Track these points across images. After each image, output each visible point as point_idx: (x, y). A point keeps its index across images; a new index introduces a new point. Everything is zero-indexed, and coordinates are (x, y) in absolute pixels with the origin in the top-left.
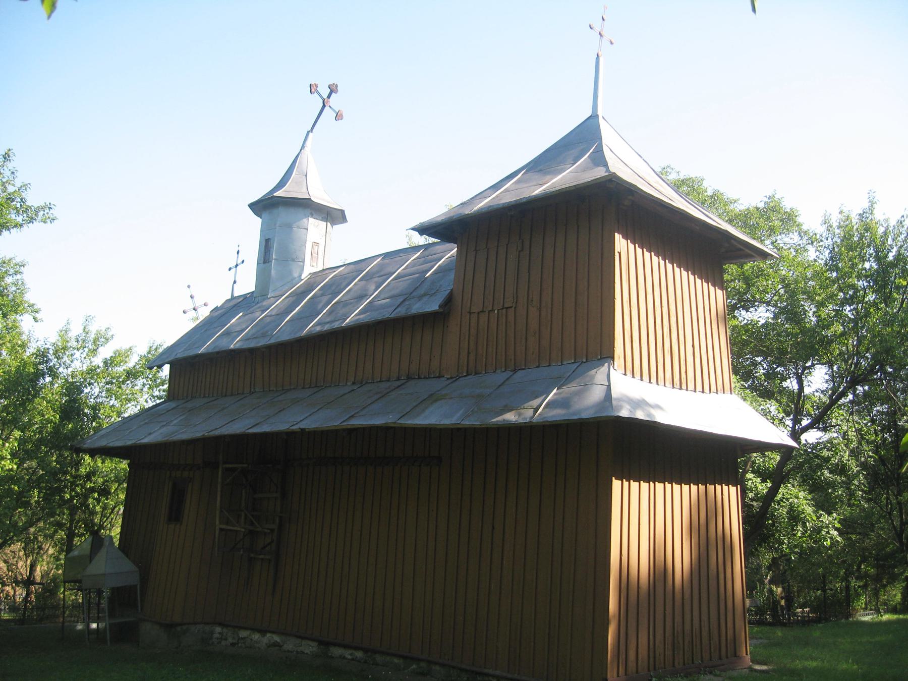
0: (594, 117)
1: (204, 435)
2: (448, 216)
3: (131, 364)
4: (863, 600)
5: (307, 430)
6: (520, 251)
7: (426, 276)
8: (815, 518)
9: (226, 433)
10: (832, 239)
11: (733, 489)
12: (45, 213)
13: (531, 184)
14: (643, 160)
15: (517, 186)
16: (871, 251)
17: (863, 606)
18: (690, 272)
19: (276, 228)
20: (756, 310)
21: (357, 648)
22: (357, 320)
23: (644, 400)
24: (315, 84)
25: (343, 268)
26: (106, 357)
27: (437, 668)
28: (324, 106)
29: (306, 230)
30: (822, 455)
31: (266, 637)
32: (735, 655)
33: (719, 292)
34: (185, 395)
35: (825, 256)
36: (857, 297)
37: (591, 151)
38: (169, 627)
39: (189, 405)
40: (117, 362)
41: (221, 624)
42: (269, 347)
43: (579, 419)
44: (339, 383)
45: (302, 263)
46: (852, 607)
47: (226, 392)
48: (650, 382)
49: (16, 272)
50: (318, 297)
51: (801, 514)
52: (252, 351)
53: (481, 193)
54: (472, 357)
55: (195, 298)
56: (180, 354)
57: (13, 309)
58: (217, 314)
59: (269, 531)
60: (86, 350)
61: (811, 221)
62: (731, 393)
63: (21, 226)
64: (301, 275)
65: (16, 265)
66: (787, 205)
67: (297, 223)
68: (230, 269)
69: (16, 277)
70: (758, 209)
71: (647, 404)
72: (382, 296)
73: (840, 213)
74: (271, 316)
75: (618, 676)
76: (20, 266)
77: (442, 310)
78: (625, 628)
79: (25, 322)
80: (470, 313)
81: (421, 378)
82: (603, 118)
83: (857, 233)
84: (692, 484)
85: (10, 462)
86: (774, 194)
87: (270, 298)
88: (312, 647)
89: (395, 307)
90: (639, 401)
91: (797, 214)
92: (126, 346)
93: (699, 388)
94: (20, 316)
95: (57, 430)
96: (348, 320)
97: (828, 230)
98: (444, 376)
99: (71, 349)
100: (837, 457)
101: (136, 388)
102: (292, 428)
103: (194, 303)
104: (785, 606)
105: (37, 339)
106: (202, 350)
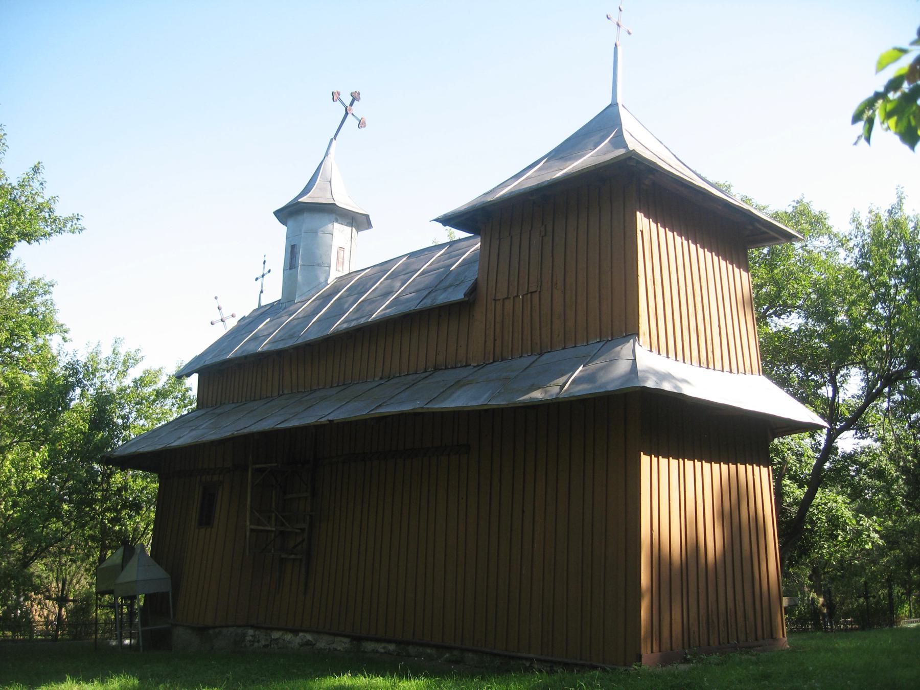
0: (614, 105)
1: (233, 434)
2: (471, 205)
3: (159, 385)
4: (907, 607)
5: (335, 422)
6: (543, 237)
7: (452, 269)
8: (854, 522)
9: (255, 430)
10: (861, 237)
11: (764, 470)
12: (74, 224)
13: (552, 170)
14: (664, 146)
15: (538, 174)
16: (902, 248)
17: (907, 614)
18: (714, 253)
19: (301, 234)
20: (788, 316)
21: (389, 641)
22: (384, 314)
23: (670, 374)
24: (338, 92)
25: (369, 270)
26: (136, 377)
27: (470, 655)
28: (347, 114)
30: (860, 460)
31: (298, 637)
32: (772, 638)
33: (744, 274)
34: (214, 402)
35: (854, 254)
36: (889, 294)
37: (611, 136)
38: (201, 630)
39: (218, 411)
40: (147, 382)
42: (297, 349)
43: (606, 392)
44: (366, 380)
45: (328, 268)
46: (896, 614)
47: (255, 396)
48: (676, 360)
49: (45, 291)
50: (344, 298)
51: (840, 518)
53: (504, 183)
54: (498, 343)
55: (222, 310)
56: (209, 361)
57: (43, 329)
58: (244, 323)
59: (299, 531)
61: (840, 224)
62: (759, 375)
63: (50, 234)
64: (327, 280)
65: (45, 285)
66: (815, 209)
67: (322, 229)
68: (257, 279)
69: (45, 298)
70: (786, 213)
71: (673, 378)
72: (408, 291)
73: (869, 212)
74: (298, 319)
75: (652, 652)
76: (49, 286)
77: (467, 299)
78: (657, 603)
79: (54, 341)
81: (449, 369)
83: (887, 230)
84: (722, 463)
85: (41, 472)
86: (802, 198)
87: (297, 303)
88: (345, 643)
90: (665, 374)
91: (826, 217)
92: (156, 367)
93: (727, 368)
94: (50, 336)
95: (88, 437)
96: (374, 316)
97: (857, 228)
98: (471, 365)
99: (101, 370)
100: (876, 462)
101: (166, 407)
104: (826, 614)
105: (66, 353)
106: (230, 356)
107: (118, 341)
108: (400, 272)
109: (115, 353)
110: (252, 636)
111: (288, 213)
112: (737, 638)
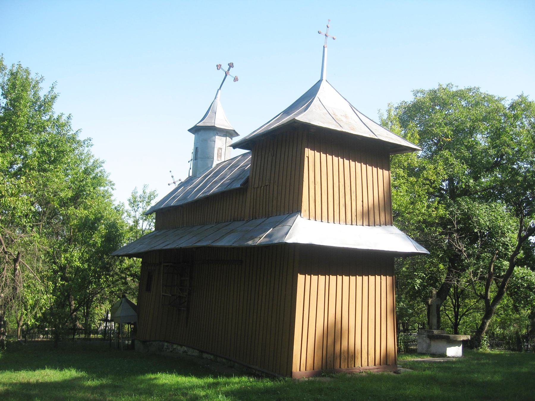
21: (211, 354)
24: (219, 65)
28: (226, 75)
29: (214, 142)
38: (144, 342)
41: (167, 342)
45: (212, 160)
52: (181, 206)
68: (189, 162)
72: (229, 179)
80: (254, 188)
82: (326, 81)
96: (211, 192)
103: (174, 179)
107: (146, 186)
109: (144, 192)
110: (167, 346)
111: (195, 130)
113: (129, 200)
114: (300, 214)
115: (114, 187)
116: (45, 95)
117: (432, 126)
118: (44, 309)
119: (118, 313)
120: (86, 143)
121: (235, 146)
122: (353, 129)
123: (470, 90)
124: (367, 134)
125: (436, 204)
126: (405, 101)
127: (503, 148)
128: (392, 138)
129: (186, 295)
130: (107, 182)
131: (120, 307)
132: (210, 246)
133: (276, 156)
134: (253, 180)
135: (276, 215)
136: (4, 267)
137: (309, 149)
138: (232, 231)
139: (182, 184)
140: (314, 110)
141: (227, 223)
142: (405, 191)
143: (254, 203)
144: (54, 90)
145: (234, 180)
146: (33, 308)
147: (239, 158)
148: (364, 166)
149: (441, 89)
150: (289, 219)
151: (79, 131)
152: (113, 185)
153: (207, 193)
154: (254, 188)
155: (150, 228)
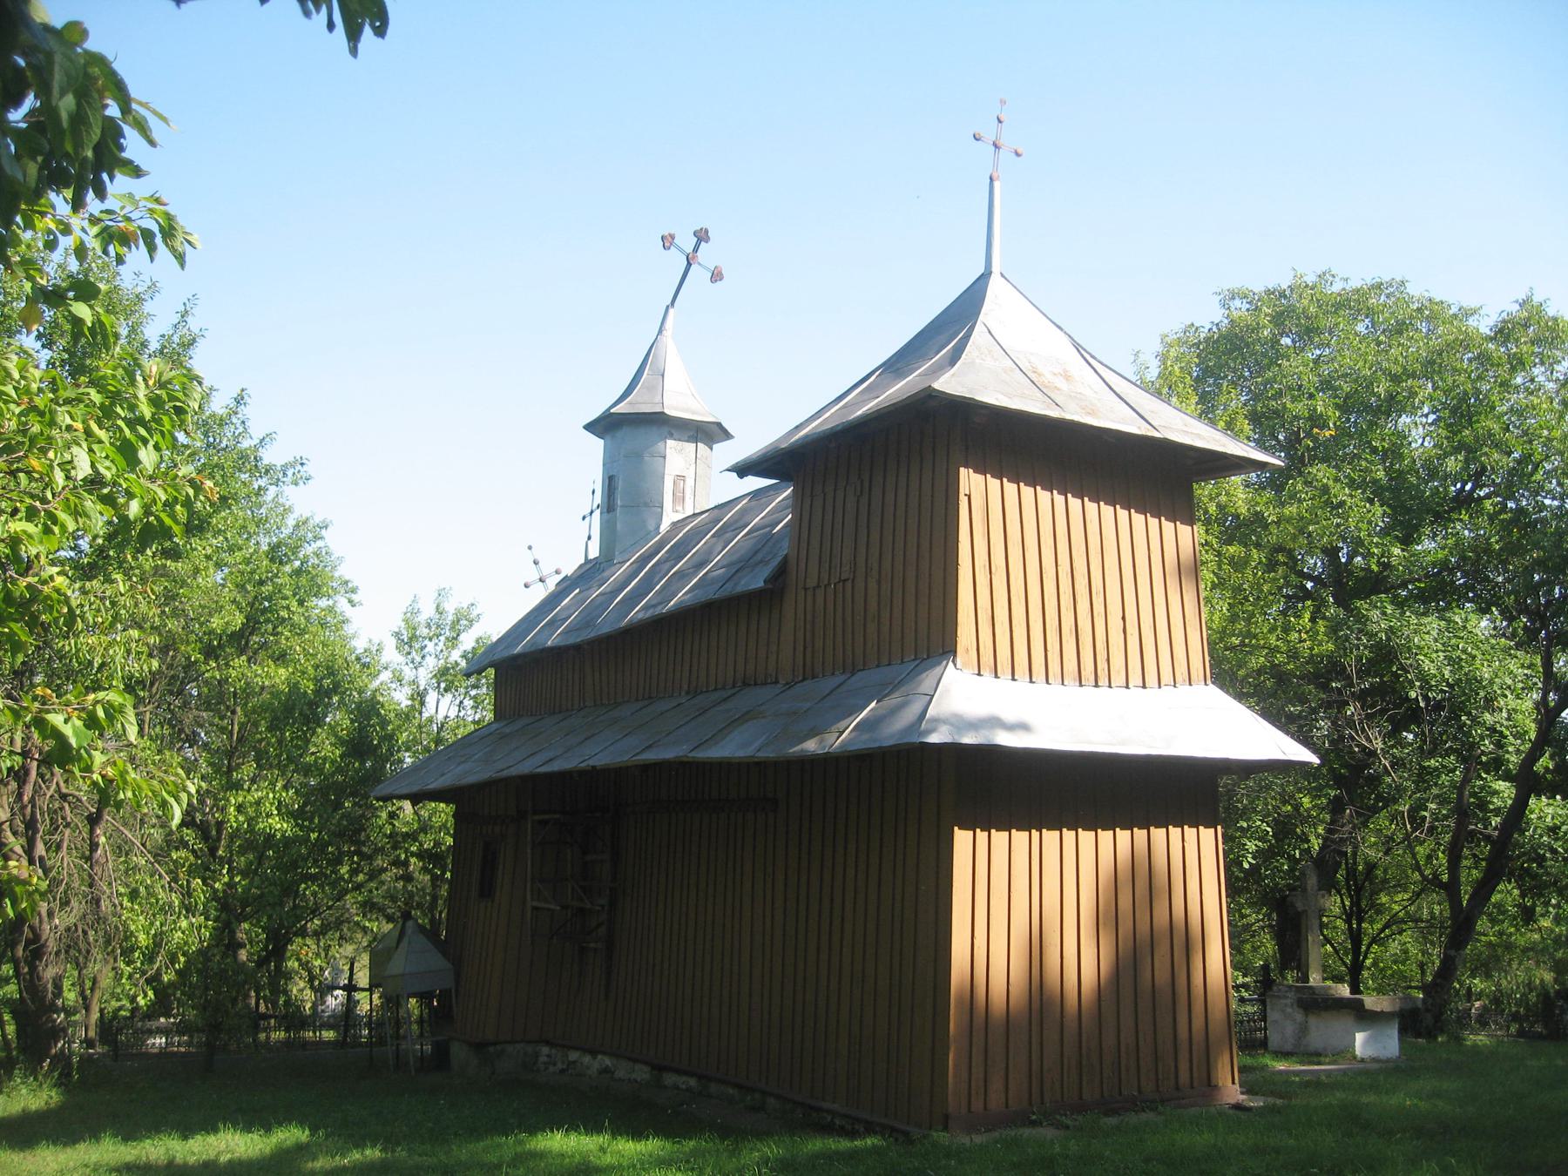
11: (1207, 834)
24: (670, 235)
28: (689, 264)
38: (479, 1047)
41: (547, 1043)
43: (880, 748)
52: (577, 647)
56: (499, 655)
60: (442, 638)
62: (1206, 684)
68: (584, 518)
72: (720, 565)
89: (720, 584)
96: (672, 603)
102: (582, 765)
103: (539, 570)
107: (443, 593)
108: (731, 525)
109: (439, 610)
111: (605, 425)
112: (1139, 1086)
113: (397, 633)
114: (953, 661)
115: (354, 597)
116: (163, 336)
117: (1279, 394)
118: (182, 959)
119: (397, 965)
120: (290, 473)
121: (743, 470)
122: (1091, 414)
123: (1378, 287)
124: (1132, 426)
125: (1307, 620)
126: (1196, 325)
127: (1486, 454)
128: (1198, 436)
129: (603, 906)
130: (334, 584)
131: (401, 945)
132: (685, 759)
133: (870, 494)
134: (802, 565)
135: (878, 666)
136: (62, 841)
137: (971, 471)
138: (746, 717)
139: (566, 586)
140: (977, 361)
141: (725, 694)
142: (1209, 585)
143: (808, 634)
144: (189, 319)
145: (741, 565)
146: (150, 958)
147: (744, 502)
148: (1123, 514)
149: (1298, 288)
150: (926, 670)
151: (268, 439)
152: (354, 591)
153: (660, 607)
154: (806, 589)
155: (461, 714)
